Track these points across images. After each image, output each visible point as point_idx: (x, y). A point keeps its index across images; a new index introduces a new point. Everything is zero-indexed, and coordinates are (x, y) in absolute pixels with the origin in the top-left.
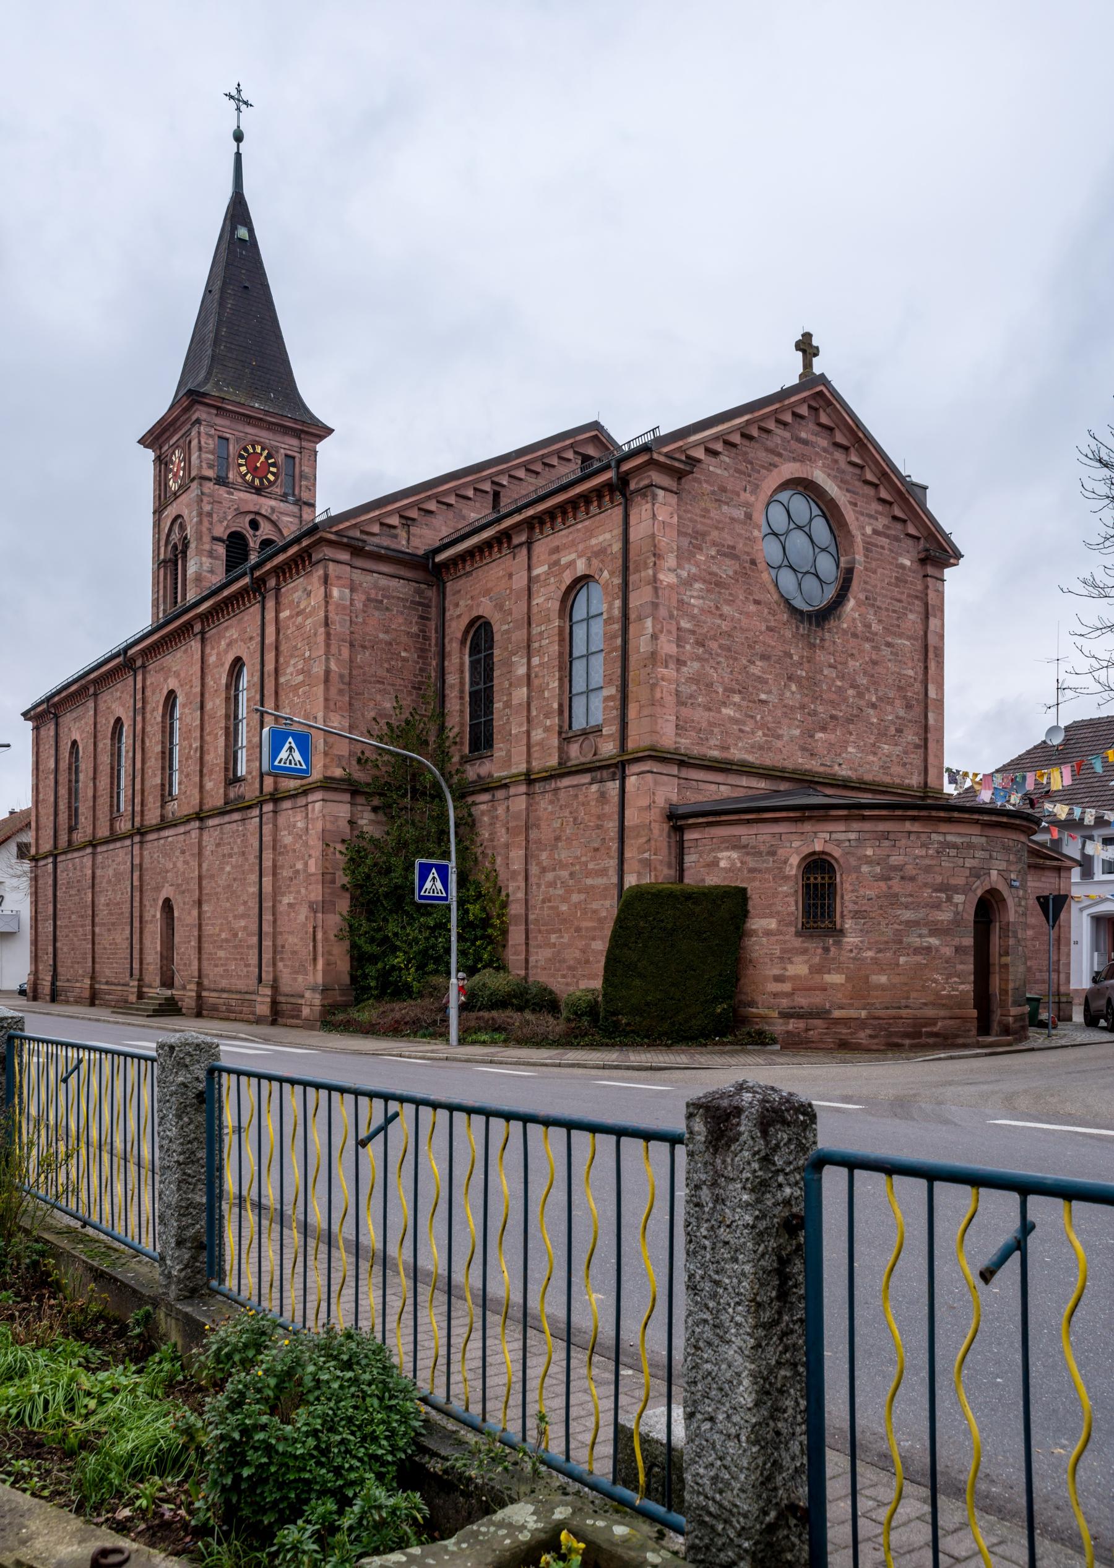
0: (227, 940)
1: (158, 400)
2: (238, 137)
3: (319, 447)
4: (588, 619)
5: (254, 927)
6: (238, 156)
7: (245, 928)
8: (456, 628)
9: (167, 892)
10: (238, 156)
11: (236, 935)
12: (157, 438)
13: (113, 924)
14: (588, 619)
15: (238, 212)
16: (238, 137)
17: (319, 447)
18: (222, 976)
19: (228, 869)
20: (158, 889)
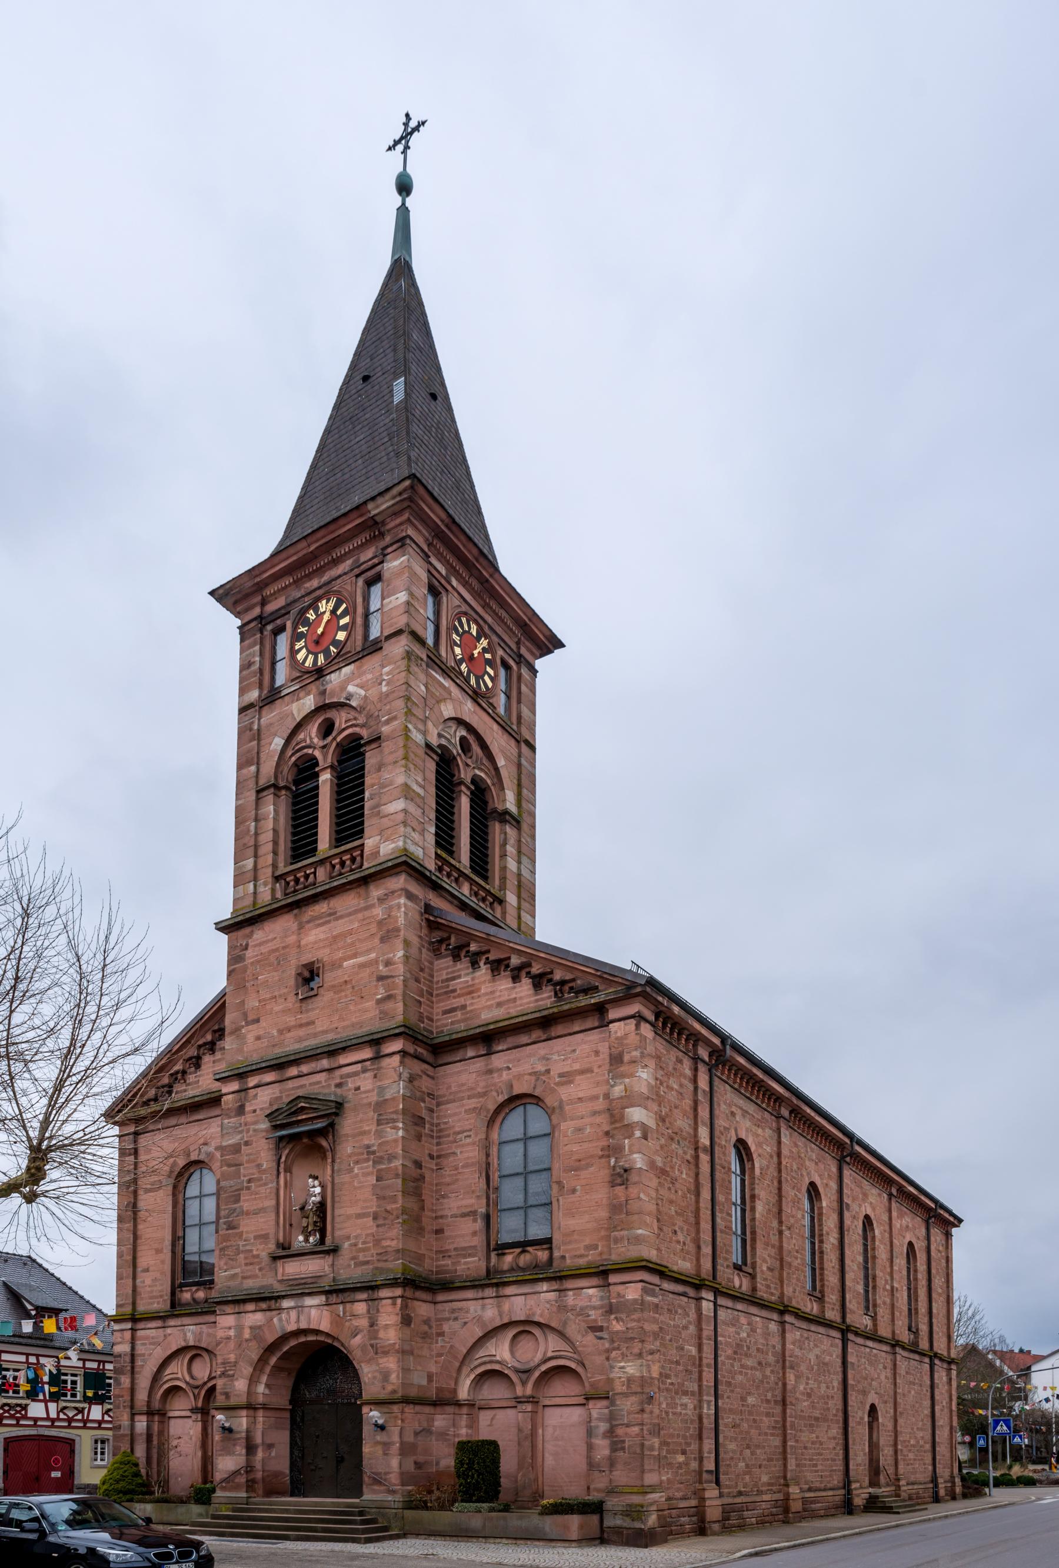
0: (913, 1446)
1: (256, 533)
2: (404, 187)
3: (539, 664)
4: (201, 1196)
5: (929, 1437)
6: (403, 213)
7: (922, 1438)
8: (279, 622)
9: (872, 1398)
10: (403, 213)
11: (918, 1442)
12: (257, 600)
13: (817, 1419)
14: (201, 1196)
15: (401, 270)
16: (404, 187)
17: (539, 664)
18: (912, 1473)
19: (913, 1392)
20: (864, 1393)
